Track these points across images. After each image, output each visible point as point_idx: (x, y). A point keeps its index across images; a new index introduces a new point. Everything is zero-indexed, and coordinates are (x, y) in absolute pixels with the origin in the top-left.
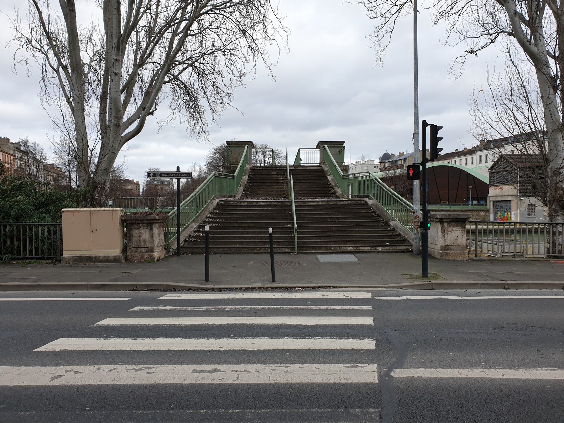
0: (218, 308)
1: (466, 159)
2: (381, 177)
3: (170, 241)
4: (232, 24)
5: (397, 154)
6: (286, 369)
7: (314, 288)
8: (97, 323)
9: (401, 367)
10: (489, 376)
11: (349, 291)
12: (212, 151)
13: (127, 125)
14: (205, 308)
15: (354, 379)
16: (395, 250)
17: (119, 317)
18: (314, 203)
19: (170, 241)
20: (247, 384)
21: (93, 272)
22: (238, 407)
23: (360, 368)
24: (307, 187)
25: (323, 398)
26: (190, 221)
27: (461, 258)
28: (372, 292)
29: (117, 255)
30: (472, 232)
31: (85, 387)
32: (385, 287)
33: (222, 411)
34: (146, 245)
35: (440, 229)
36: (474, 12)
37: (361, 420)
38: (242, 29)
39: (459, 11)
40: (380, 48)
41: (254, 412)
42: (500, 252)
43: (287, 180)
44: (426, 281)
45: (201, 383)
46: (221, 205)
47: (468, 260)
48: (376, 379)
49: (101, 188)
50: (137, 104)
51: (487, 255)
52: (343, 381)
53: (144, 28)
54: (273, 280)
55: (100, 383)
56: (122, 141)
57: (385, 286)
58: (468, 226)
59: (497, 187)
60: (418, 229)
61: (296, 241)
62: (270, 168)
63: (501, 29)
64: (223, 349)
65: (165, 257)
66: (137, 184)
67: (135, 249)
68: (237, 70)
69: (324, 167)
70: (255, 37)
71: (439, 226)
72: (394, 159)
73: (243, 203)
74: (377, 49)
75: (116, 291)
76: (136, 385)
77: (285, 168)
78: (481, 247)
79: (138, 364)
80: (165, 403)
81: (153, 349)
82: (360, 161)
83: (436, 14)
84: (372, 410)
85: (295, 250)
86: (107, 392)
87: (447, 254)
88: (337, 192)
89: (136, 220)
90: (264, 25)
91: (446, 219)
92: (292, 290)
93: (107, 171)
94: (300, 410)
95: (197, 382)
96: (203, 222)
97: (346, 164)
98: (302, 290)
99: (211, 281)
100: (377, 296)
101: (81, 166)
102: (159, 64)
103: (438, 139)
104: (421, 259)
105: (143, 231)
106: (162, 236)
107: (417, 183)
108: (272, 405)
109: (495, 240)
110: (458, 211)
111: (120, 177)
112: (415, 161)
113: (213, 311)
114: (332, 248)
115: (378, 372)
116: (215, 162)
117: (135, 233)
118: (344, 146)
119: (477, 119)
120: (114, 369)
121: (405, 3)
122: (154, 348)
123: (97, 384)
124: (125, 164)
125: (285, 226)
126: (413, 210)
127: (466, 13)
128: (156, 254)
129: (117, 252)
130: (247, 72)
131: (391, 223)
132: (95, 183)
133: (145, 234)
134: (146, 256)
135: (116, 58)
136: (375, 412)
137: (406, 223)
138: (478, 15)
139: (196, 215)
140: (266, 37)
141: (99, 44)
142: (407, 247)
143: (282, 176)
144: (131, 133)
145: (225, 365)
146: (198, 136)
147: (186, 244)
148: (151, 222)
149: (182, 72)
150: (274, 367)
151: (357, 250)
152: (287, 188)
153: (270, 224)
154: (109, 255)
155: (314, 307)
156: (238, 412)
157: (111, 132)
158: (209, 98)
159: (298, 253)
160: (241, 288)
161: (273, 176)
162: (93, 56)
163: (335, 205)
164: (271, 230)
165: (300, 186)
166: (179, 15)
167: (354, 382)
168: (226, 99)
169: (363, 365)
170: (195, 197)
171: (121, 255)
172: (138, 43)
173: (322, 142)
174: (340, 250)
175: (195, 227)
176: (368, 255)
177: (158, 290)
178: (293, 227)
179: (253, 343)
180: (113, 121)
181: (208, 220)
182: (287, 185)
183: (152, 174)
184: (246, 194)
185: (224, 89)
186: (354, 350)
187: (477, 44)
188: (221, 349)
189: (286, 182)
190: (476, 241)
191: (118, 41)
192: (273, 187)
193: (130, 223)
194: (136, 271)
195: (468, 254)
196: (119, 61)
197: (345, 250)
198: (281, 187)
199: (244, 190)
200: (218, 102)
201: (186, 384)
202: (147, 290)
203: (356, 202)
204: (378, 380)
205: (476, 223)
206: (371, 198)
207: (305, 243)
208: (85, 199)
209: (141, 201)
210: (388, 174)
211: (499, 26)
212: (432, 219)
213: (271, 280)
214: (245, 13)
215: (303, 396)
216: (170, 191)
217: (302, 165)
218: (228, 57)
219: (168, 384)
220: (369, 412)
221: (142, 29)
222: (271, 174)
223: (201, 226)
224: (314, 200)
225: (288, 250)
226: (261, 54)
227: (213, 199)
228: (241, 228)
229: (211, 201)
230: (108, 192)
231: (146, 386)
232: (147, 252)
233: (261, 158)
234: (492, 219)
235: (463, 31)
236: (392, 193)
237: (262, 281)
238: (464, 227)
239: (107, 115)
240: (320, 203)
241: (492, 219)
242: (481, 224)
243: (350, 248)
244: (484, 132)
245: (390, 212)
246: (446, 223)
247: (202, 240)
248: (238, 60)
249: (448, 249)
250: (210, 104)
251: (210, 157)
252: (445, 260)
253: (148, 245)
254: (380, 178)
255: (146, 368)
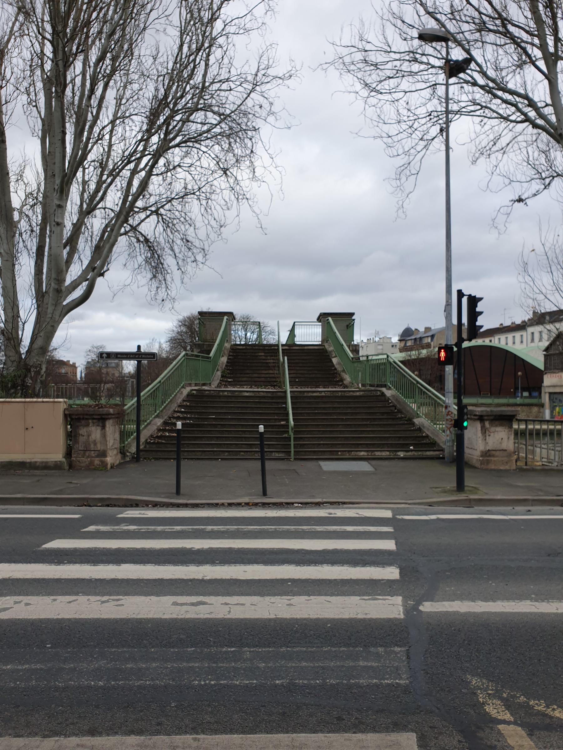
0: (196, 529)
1: (514, 337)
2: (401, 359)
3: (126, 443)
4: (210, 161)
5: (422, 329)
6: (289, 602)
7: (318, 505)
8: (44, 546)
9: (432, 601)
10: (540, 611)
11: (363, 508)
12: (176, 323)
13: (70, 290)
14: (179, 528)
15: (374, 615)
16: (421, 456)
17: (70, 538)
18: (315, 394)
19: (126, 443)
20: (242, 620)
21: (28, 481)
22: (233, 645)
23: (380, 601)
24: (305, 372)
25: (337, 635)
26: (153, 416)
27: (507, 467)
28: (392, 509)
29: (59, 460)
30: (521, 434)
31: (41, 621)
32: (409, 504)
33: (213, 650)
34: (97, 448)
35: (480, 429)
36: (522, 150)
37: (384, 660)
38: (222, 166)
39: (502, 149)
40: (403, 195)
41: (253, 651)
42: (557, 459)
43: (278, 363)
44: (462, 496)
45: (184, 618)
46: (193, 395)
47: (516, 469)
48: (402, 614)
49: (35, 372)
50: (82, 262)
51: (540, 463)
52: (360, 616)
53: (93, 164)
54: (265, 494)
55: (59, 617)
56: (64, 311)
57: (409, 502)
58: (515, 426)
59: (554, 375)
60: (451, 429)
61: (292, 443)
62: (257, 348)
63: (556, 172)
64: (208, 578)
65: (120, 464)
66: (74, 366)
67: (82, 452)
68: (215, 219)
69: (327, 347)
70: (239, 178)
71: (478, 425)
72: (418, 336)
73: (221, 393)
74: (399, 195)
75: (61, 506)
76: (104, 620)
77: (276, 348)
78: (533, 452)
79: (103, 595)
80: (142, 640)
81: (119, 578)
82: (373, 338)
83: (473, 151)
84: (397, 649)
85: (290, 456)
86: (69, 627)
87: (488, 462)
88: (345, 380)
89: (83, 415)
90: (252, 162)
91: (488, 416)
92: (289, 506)
93: (45, 349)
94: (310, 649)
95: (180, 617)
96: (170, 418)
97: (355, 343)
98: (302, 507)
99: (183, 495)
100: (399, 515)
101: (10, 343)
102: (112, 210)
103: (477, 314)
104: (455, 468)
105: (93, 429)
106: (117, 436)
107: (449, 369)
108: (274, 643)
109: (550, 444)
110: (503, 405)
111: (53, 357)
112: (447, 340)
113: (190, 532)
114: (339, 453)
115: (403, 605)
116: (180, 337)
117: (83, 431)
118: (354, 320)
119: (527, 286)
120: (74, 601)
121: (434, 138)
122: (120, 577)
123: (55, 617)
124: (67, 341)
125: (278, 424)
126: (444, 403)
127: (512, 150)
128: (109, 460)
129: (58, 456)
130: (228, 222)
131: (416, 421)
132: (28, 365)
133: (95, 433)
134: (97, 461)
135: (58, 203)
136: (401, 651)
137: (434, 420)
138: (528, 153)
139: (161, 409)
140: (254, 178)
141: (34, 186)
142: (437, 453)
143: (272, 358)
144: (77, 301)
145: (212, 597)
146: (162, 305)
147: (148, 446)
148: (103, 417)
149: (142, 221)
150: (273, 599)
151: (371, 455)
152: (279, 374)
153: (261, 421)
154: (48, 460)
155: (319, 528)
156: (234, 651)
157: (49, 300)
158: (177, 255)
159: (295, 459)
160: (223, 504)
161: (261, 358)
162: (26, 199)
163: (342, 397)
164: (261, 428)
165: (295, 372)
166: (141, 148)
167: (374, 617)
168: (200, 258)
169: (384, 597)
170: (159, 384)
171: (64, 460)
172: (85, 183)
173: (325, 314)
174: (349, 455)
175: (159, 424)
176: (386, 463)
177: (115, 506)
178: (288, 425)
179: (245, 571)
180: (53, 284)
181: (175, 416)
182: (279, 370)
183: (105, 355)
184: (226, 381)
185: (197, 243)
186: (373, 580)
187: (527, 190)
188: (205, 578)
189: (278, 366)
190: (526, 445)
191: (62, 182)
192: (260, 372)
193: (76, 419)
194: (85, 481)
195: (516, 461)
196: (61, 207)
197: (356, 455)
198: (271, 372)
199: (222, 376)
200: (189, 260)
201: (166, 619)
202: (100, 505)
203: (370, 393)
204: (404, 615)
205: (526, 421)
206: (390, 387)
207: (302, 446)
208: (14, 386)
209: (79, 389)
210: (410, 356)
211: (553, 168)
212: (469, 416)
213: (262, 493)
214: (226, 146)
215: (312, 632)
216: (119, 376)
217: (298, 343)
218: (204, 202)
219: (144, 619)
220: (394, 651)
221: (90, 165)
222: (257, 354)
223: (169, 424)
224: (314, 389)
225: (281, 455)
226: (247, 199)
227: (183, 387)
228: (219, 426)
229: (180, 390)
230: (44, 378)
231: (116, 621)
232: (97, 456)
233: (242, 333)
234: (547, 417)
235: (508, 173)
236: (418, 382)
237: (250, 495)
238: (511, 427)
239: (44, 277)
240: (323, 394)
241: (547, 417)
242: (532, 422)
243: (362, 453)
244: (536, 303)
245: (414, 406)
246: (488, 422)
247: (168, 441)
248: (218, 207)
249: (490, 456)
250: (178, 263)
251: (173, 331)
252: (487, 470)
253: (99, 447)
254: (400, 362)
255: (113, 600)
